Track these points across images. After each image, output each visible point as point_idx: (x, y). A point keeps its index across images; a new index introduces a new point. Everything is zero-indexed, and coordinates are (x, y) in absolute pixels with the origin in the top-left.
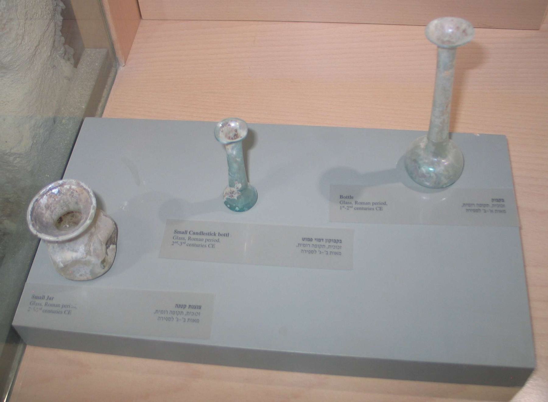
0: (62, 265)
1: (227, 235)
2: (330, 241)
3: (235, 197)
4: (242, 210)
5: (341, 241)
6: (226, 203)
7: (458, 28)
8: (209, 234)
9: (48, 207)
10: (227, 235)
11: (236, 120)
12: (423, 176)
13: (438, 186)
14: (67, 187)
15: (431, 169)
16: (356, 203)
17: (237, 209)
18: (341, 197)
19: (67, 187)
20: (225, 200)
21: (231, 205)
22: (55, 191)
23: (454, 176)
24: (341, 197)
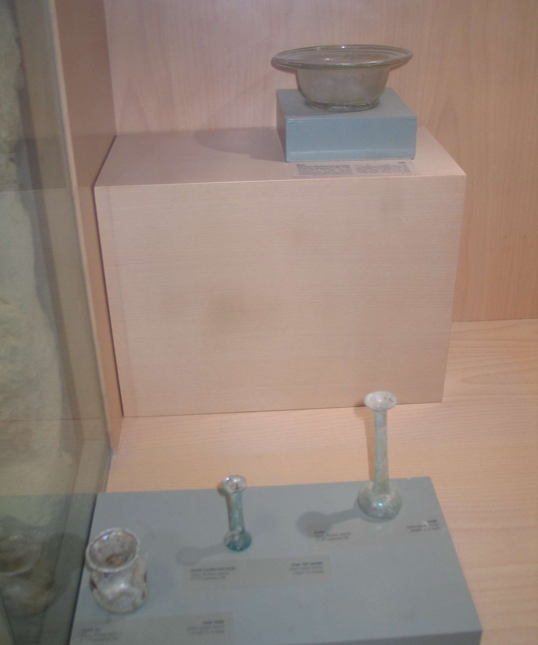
0: (110, 597)
1: (233, 568)
2: (313, 564)
3: (237, 538)
4: (242, 549)
5: (322, 563)
6: (228, 546)
7: (385, 398)
8: (219, 569)
9: (100, 550)
10: (233, 568)
11: (237, 476)
12: (375, 509)
13: (387, 517)
14: (114, 534)
15: (381, 504)
16: (328, 535)
17: (238, 548)
18: (316, 532)
19: (114, 534)
20: (227, 542)
21: (232, 546)
22: (105, 538)
23: (397, 508)
24: (316, 532)
